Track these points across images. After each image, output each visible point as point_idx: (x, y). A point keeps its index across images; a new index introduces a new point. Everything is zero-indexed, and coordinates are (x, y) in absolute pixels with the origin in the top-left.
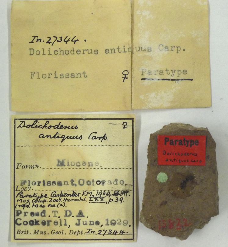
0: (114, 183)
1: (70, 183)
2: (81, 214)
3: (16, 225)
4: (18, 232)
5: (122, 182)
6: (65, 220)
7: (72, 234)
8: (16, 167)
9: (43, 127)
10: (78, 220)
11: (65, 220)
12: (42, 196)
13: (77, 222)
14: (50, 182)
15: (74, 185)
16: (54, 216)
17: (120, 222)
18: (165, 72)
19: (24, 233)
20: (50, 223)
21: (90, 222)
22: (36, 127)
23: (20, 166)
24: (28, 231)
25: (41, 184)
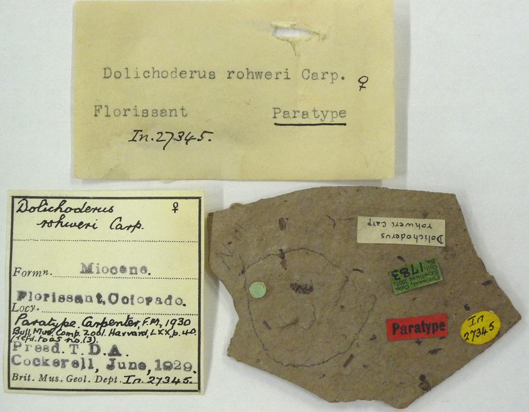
0: (165, 302)
1: (95, 299)
2: (115, 352)
3: (12, 365)
4: (14, 376)
5: (179, 301)
8: (13, 274)
9: (56, 210)
10: (111, 359)
12: (65, 324)
14: (64, 296)
16: (72, 353)
17: (180, 364)
18: (311, 115)
19: (23, 379)
20: (66, 363)
21: (131, 364)
22: (45, 210)
23: (19, 272)
24: (29, 376)
25: (50, 299)
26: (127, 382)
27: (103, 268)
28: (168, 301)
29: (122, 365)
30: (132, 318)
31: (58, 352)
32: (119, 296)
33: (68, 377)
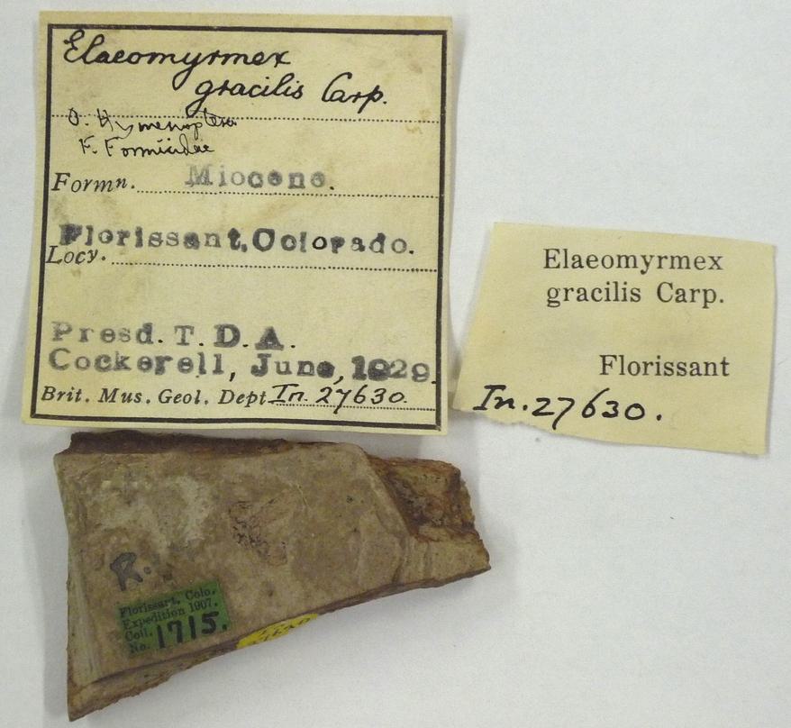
0: (371, 248)
1: (226, 242)
4: (46, 392)
5: (399, 246)
6: (216, 356)
7: (230, 401)
10: (260, 356)
11: (216, 356)
13: (259, 363)
15: (240, 249)
19: (65, 398)
20: (166, 364)
21: (302, 364)
22: (103, 58)
23: (65, 182)
26: (279, 400)
27: (233, 174)
28: (377, 246)
29: (283, 368)
30: (645, 373)
31: (149, 341)
32: (276, 235)
33: (162, 393)
